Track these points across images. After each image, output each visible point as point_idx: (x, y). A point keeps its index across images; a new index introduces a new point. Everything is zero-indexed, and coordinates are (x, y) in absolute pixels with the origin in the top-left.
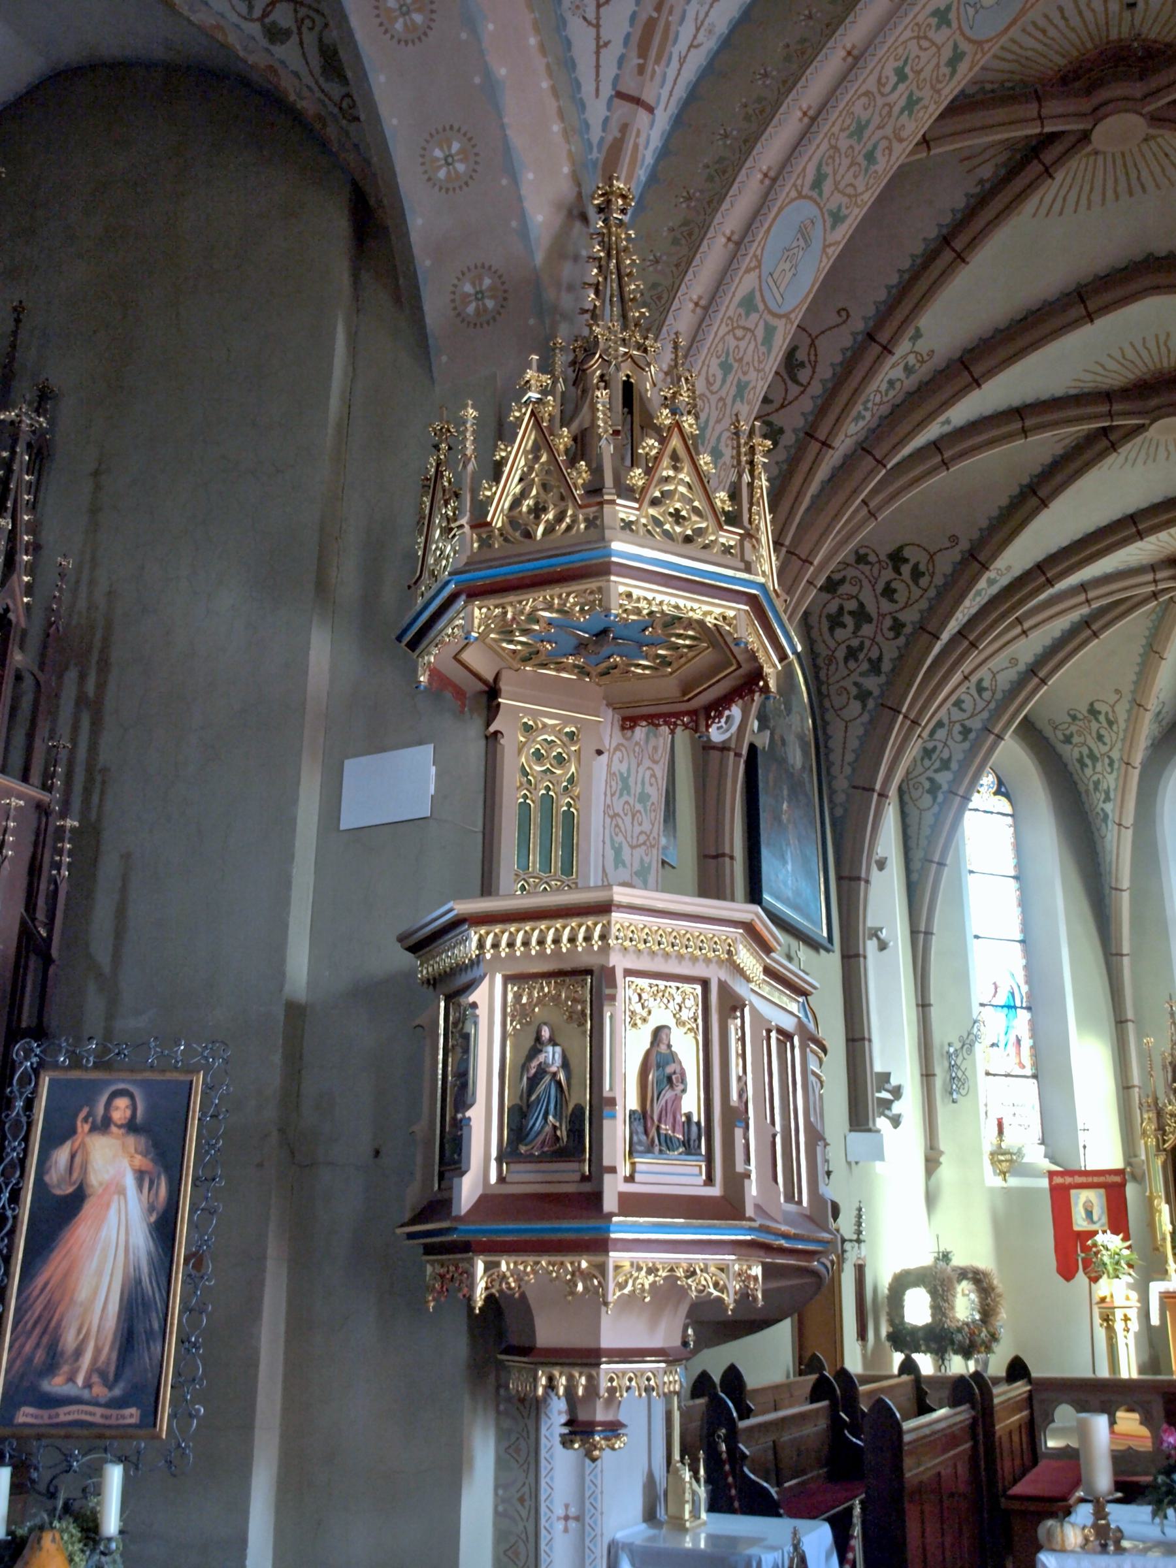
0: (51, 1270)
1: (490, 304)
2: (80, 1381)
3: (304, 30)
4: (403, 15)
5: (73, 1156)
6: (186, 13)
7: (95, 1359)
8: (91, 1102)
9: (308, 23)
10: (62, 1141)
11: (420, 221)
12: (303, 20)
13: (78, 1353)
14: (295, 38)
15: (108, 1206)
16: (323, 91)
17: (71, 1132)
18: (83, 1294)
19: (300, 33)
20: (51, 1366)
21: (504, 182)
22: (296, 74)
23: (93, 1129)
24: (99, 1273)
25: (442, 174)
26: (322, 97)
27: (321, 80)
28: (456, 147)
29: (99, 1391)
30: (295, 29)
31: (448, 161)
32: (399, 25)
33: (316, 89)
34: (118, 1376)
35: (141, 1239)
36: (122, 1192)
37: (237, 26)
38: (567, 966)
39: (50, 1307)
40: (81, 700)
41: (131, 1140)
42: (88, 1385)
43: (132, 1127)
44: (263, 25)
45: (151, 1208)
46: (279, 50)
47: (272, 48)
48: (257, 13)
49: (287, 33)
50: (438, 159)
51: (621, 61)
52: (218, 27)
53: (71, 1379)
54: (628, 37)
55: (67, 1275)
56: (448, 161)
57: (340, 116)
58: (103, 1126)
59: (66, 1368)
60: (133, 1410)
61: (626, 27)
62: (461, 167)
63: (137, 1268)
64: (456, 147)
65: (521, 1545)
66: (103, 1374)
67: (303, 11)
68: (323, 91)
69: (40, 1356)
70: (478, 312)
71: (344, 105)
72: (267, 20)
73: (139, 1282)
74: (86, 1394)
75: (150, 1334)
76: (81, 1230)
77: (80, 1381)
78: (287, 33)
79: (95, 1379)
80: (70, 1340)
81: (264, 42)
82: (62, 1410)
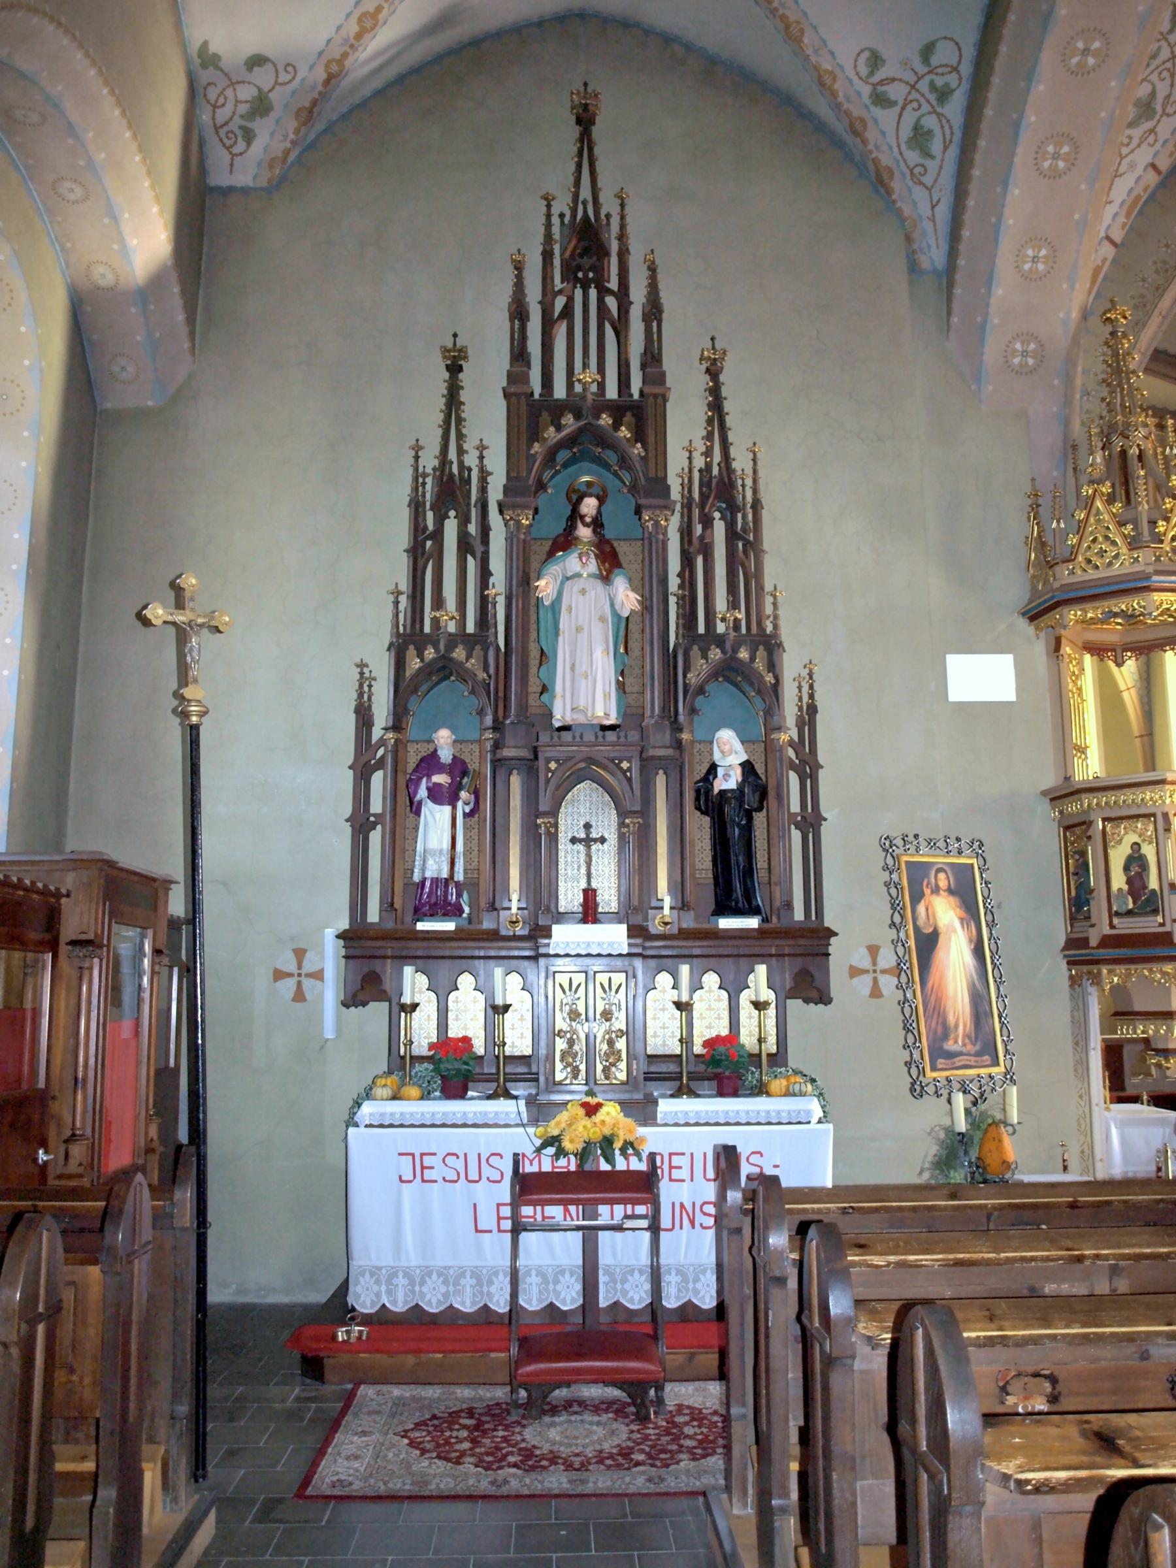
0: (932, 980)
1: (1031, 361)
2: (960, 1042)
3: (909, 107)
4: (1053, 158)
5: (927, 909)
6: (809, 51)
7: (964, 1030)
8: (927, 876)
9: (915, 105)
10: (919, 901)
11: (1000, 292)
12: (911, 101)
13: (956, 1026)
14: (897, 109)
15: (950, 940)
16: (901, 154)
17: (922, 895)
18: (951, 992)
19: (903, 108)
20: (946, 1036)
21: (1065, 286)
22: (883, 133)
23: (932, 892)
24: (955, 979)
25: (1027, 267)
26: (899, 157)
27: (903, 147)
28: (1043, 252)
29: (969, 1047)
30: (900, 104)
31: (1035, 260)
32: (1046, 164)
33: (895, 149)
34: (976, 1038)
35: (969, 959)
36: (955, 931)
37: (851, 81)
38: (1077, 796)
39: (938, 1000)
40: (464, 546)
41: (952, 899)
42: (964, 1045)
43: (950, 891)
44: (874, 89)
45: (971, 941)
46: (877, 111)
47: (872, 108)
48: (876, 79)
49: (890, 104)
50: (1028, 256)
51: (1116, 215)
52: (832, 73)
53: (956, 1042)
54: (1124, 201)
55: (940, 984)
56: (1035, 260)
57: (908, 177)
58: (936, 890)
59: (952, 1036)
60: (987, 1057)
61: (1124, 196)
62: (1041, 267)
63: (971, 976)
64: (1043, 252)
65: (1082, 1121)
66: (969, 1037)
67: (914, 95)
68: (901, 154)
69: (940, 1030)
70: (1021, 365)
71: (916, 171)
72: (880, 89)
73: (974, 984)
74: (964, 1050)
75: (986, 1013)
76: (940, 954)
77: (960, 1042)
78: (890, 104)
79: (967, 1041)
80: (951, 1020)
81: (867, 101)
82: (956, 1059)
